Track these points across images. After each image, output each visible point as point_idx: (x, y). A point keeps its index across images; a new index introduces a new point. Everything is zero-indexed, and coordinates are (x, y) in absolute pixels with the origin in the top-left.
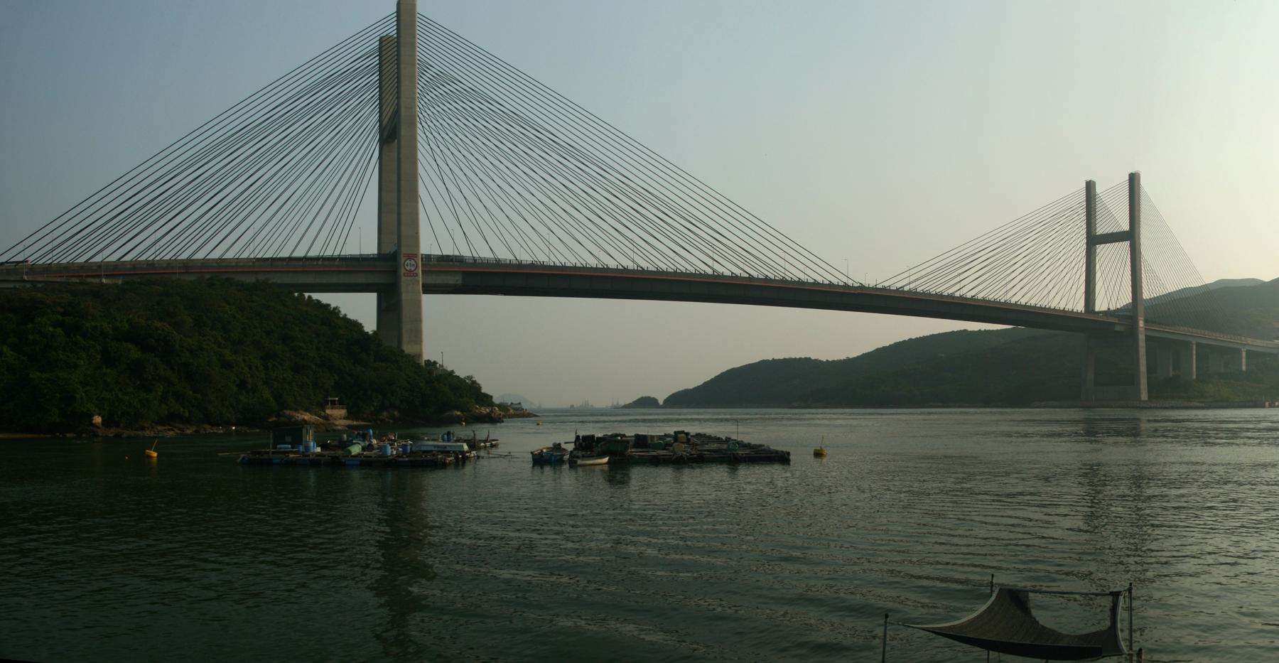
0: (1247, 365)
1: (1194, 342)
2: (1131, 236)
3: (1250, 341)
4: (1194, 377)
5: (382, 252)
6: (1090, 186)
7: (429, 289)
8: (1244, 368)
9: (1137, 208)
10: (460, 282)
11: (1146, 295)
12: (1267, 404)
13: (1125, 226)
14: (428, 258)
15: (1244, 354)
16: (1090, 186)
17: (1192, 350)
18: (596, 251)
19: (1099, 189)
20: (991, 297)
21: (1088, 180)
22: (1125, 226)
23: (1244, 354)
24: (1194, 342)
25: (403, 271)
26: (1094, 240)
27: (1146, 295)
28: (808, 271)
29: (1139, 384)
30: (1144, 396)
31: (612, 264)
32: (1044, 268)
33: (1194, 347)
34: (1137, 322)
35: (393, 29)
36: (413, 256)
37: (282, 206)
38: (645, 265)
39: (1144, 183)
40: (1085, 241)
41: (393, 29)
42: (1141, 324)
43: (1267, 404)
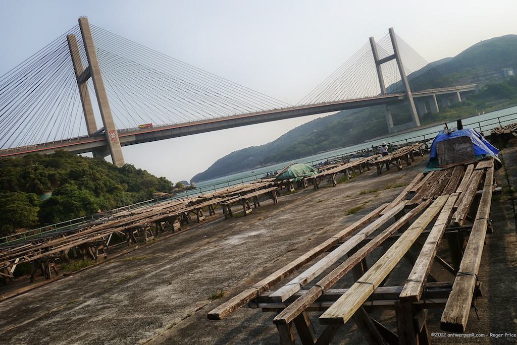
0: (461, 99)
1: (434, 95)
2: (395, 56)
3: (460, 87)
4: (438, 111)
5: (91, 133)
6: (371, 40)
7: (123, 145)
8: (460, 100)
9: (395, 43)
10: (135, 139)
11: (407, 74)
12: (479, 114)
13: (392, 53)
14: (119, 131)
15: (459, 94)
16: (371, 40)
17: (434, 99)
18: (205, 114)
19: (376, 40)
20: (349, 98)
21: (370, 37)
22: (392, 53)
23: (459, 94)
24: (434, 95)
25: (110, 139)
26: (378, 63)
27: (407, 74)
28: (278, 105)
29: (415, 120)
30: (419, 124)
31: (211, 117)
32: (363, 81)
33: (435, 97)
34: (407, 93)
35: (64, 38)
36: (114, 131)
37: (28, 123)
38: (223, 115)
39: (395, 31)
40: (375, 64)
41: (64, 38)
42: (410, 93)
43: (479, 114)
